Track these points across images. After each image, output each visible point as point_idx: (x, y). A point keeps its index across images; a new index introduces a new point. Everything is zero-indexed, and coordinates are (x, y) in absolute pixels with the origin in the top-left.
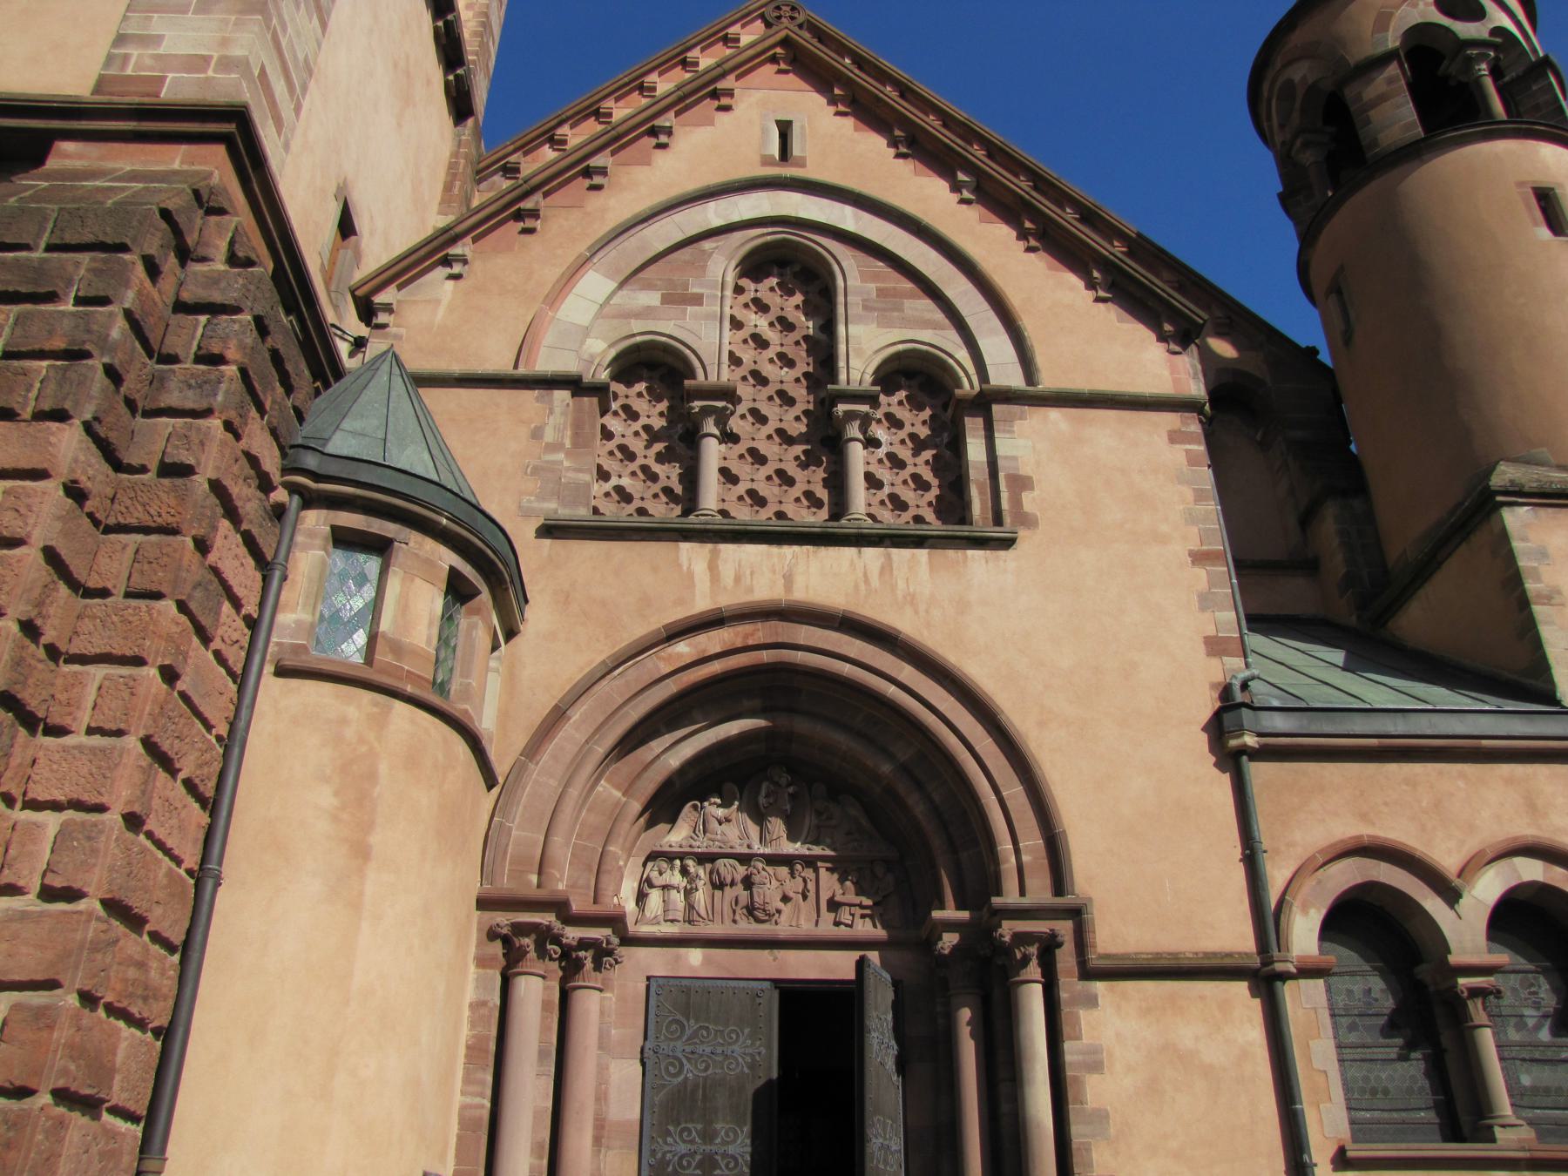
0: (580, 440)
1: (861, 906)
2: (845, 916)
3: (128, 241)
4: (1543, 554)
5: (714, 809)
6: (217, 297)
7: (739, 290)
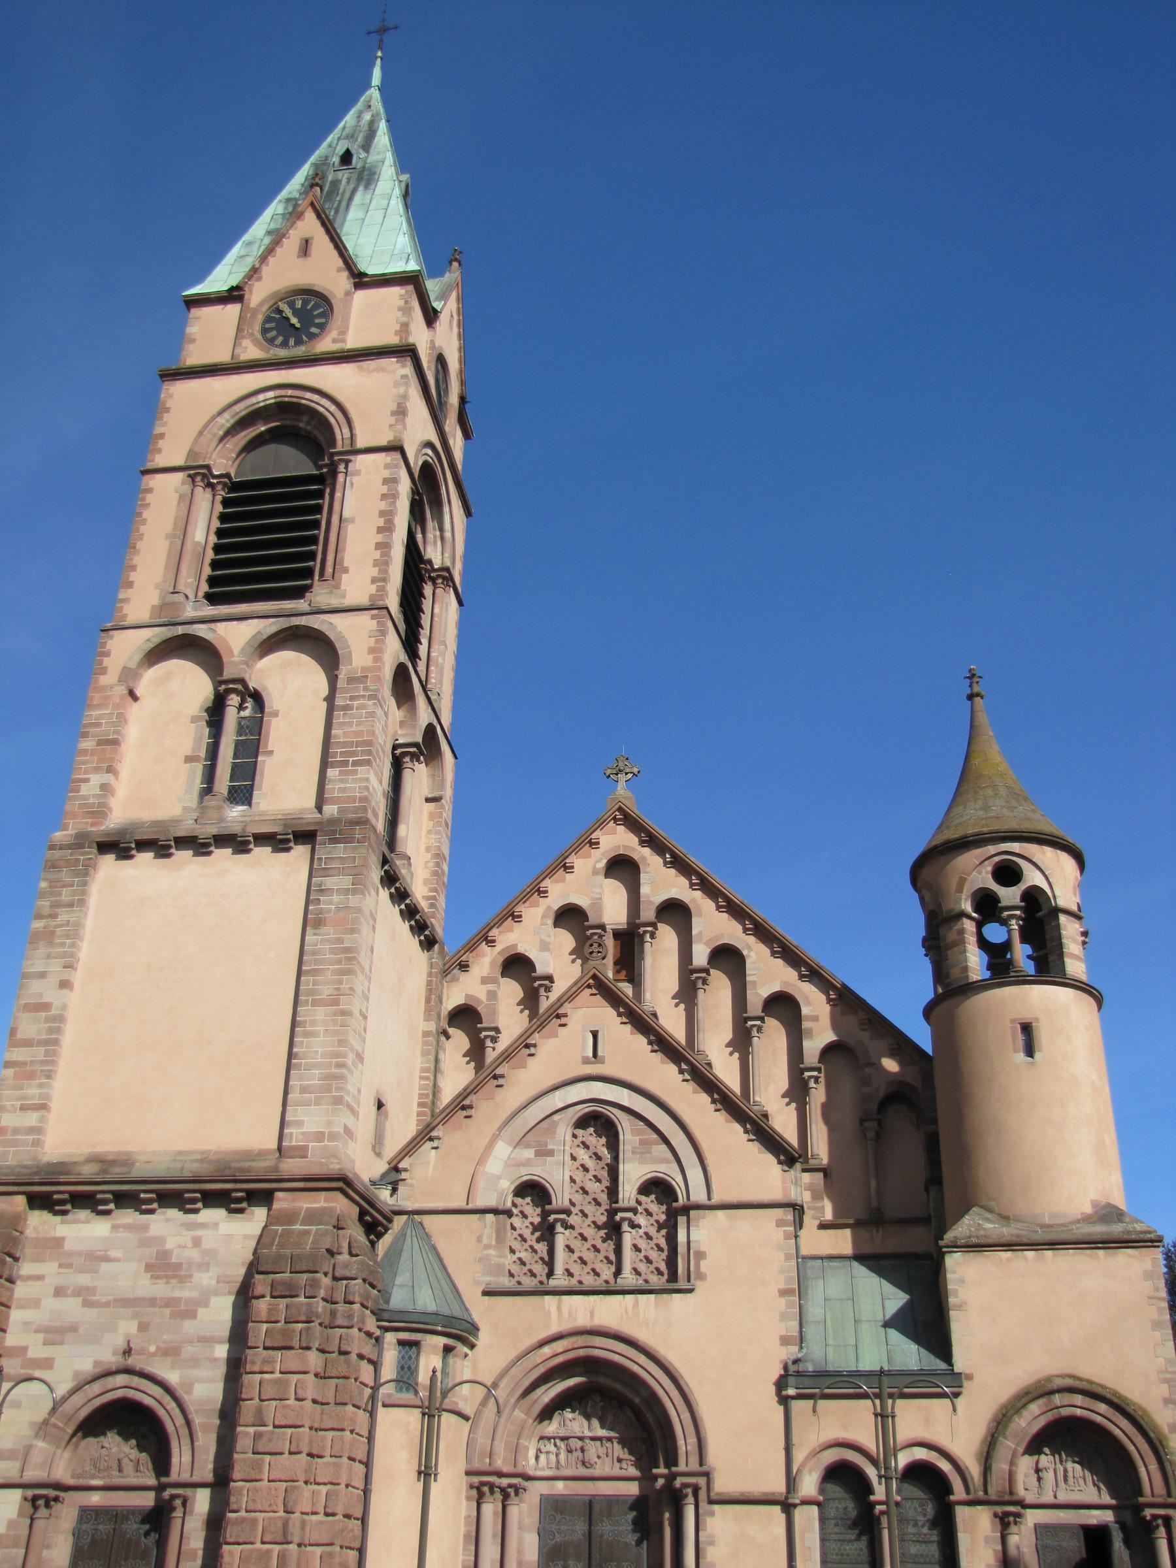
0: (500, 1239)
1: (631, 1461)
2: (624, 1466)
3: (318, 1269)
4: (962, 1281)
5: (568, 1414)
6: (348, 1274)
7: (575, 1136)
